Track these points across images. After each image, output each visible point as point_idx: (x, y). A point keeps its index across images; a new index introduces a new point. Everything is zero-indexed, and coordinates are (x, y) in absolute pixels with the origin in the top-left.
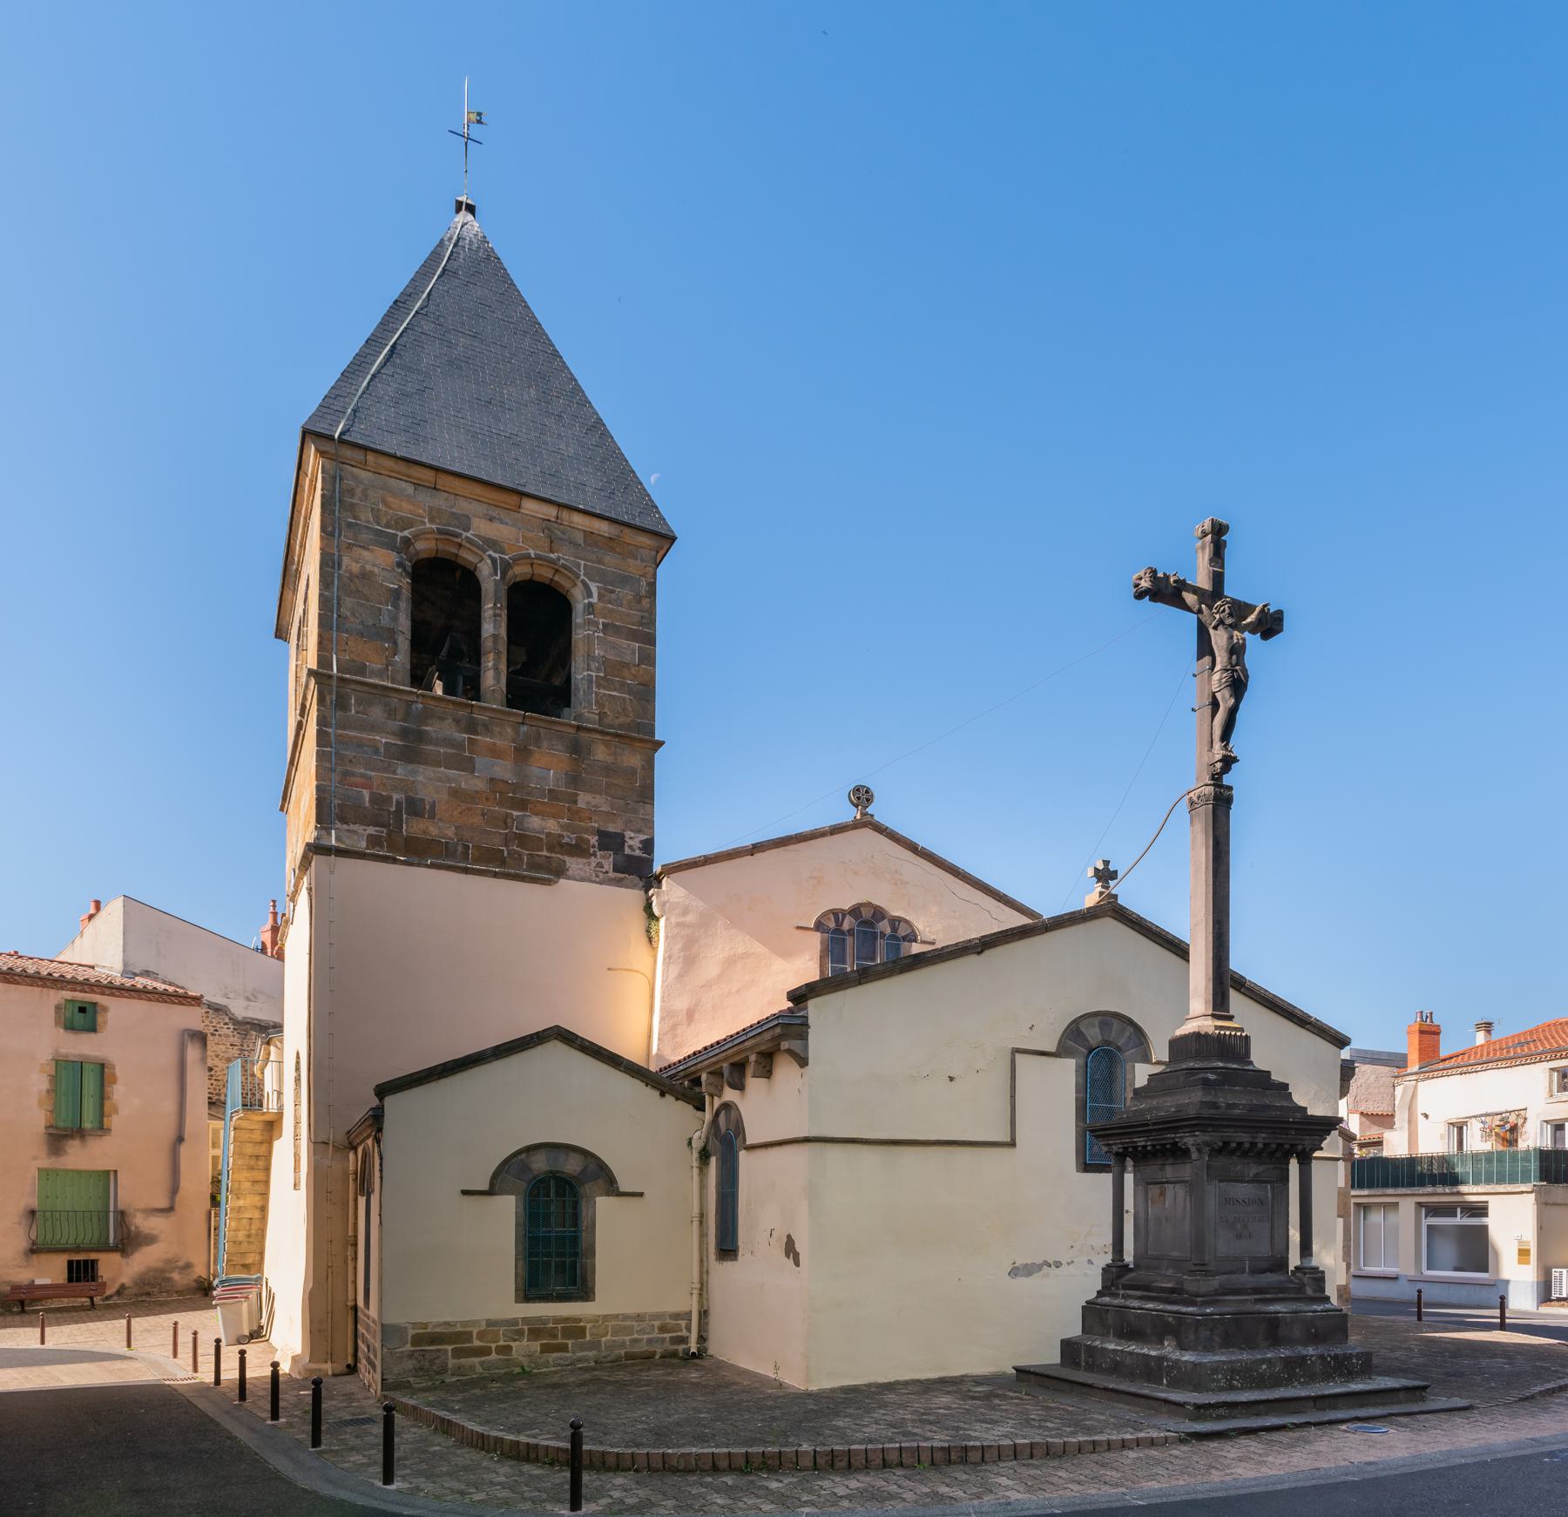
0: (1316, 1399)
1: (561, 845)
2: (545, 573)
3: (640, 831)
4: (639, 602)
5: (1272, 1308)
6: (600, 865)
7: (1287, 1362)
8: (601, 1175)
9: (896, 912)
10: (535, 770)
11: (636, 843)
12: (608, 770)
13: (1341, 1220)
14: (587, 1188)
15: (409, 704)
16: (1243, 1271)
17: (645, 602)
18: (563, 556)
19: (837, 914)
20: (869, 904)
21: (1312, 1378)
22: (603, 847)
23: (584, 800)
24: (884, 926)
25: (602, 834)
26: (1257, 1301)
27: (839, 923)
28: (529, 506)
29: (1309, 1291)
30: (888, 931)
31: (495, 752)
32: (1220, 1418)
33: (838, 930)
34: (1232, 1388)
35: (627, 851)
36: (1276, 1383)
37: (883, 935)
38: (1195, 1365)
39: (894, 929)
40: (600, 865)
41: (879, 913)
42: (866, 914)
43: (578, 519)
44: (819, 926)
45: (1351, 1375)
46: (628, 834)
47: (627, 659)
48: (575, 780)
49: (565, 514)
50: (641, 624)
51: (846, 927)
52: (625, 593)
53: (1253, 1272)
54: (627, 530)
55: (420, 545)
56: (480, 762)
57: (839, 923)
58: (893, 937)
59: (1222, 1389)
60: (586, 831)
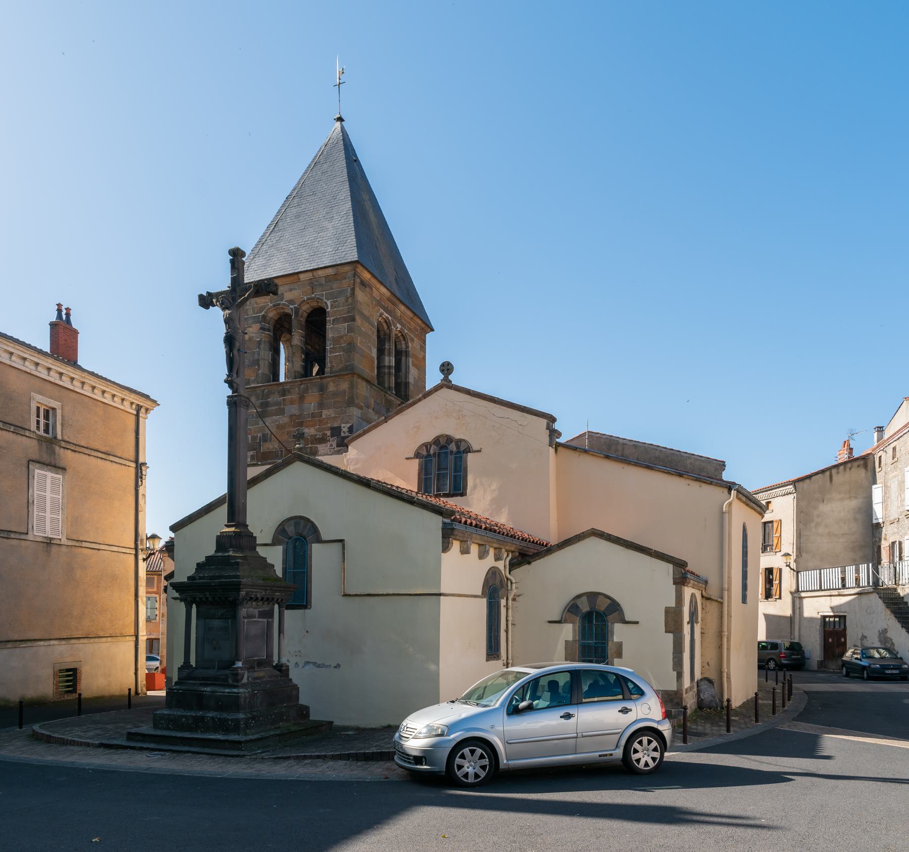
0: (182, 739)
1: (316, 439)
2: (315, 304)
3: (347, 423)
4: (347, 301)
5: (203, 689)
6: (331, 445)
7: (196, 719)
8: (615, 607)
9: (457, 437)
10: (306, 405)
11: (345, 429)
12: (335, 394)
13: (671, 636)
14: (610, 618)
15: (263, 391)
16: (214, 668)
17: (350, 300)
18: (317, 293)
19: (426, 445)
20: (442, 436)
21: (207, 730)
22: (332, 436)
23: (325, 413)
24: (453, 447)
25: (332, 429)
26: (201, 685)
27: (428, 451)
28: (302, 276)
29: (230, 681)
30: (455, 449)
31: (292, 402)
32: (138, 741)
33: (429, 455)
34: (168, 729)
35: (342, 434)
36: (189, 729)
37: (452, 452)
38: (168, 715)
39: (458, 447)
40: (331, 445)
41: (449, 439)
42: (443, 442)
43: (320, 273)
44: (417, 455)
45: (227, 731)
46: (343, 425)
47: (342, 333)
48: (321, 405)
49: (315, 273)
50: (348, 312)
51: (432, 452)
52: (341, 299)
53: (220, 668)
54: (339, 267)
55: (271, 315)
56: (287, 408)
57: (428, 451)
58: (458, 452)
59: (164, 729)
60: (326, 429)
